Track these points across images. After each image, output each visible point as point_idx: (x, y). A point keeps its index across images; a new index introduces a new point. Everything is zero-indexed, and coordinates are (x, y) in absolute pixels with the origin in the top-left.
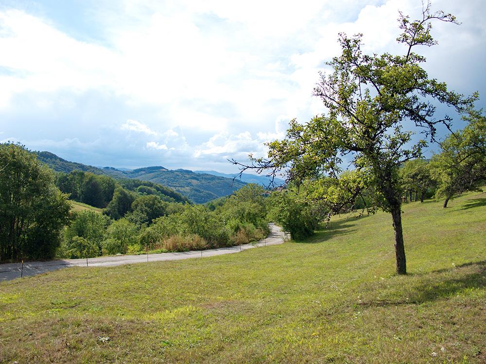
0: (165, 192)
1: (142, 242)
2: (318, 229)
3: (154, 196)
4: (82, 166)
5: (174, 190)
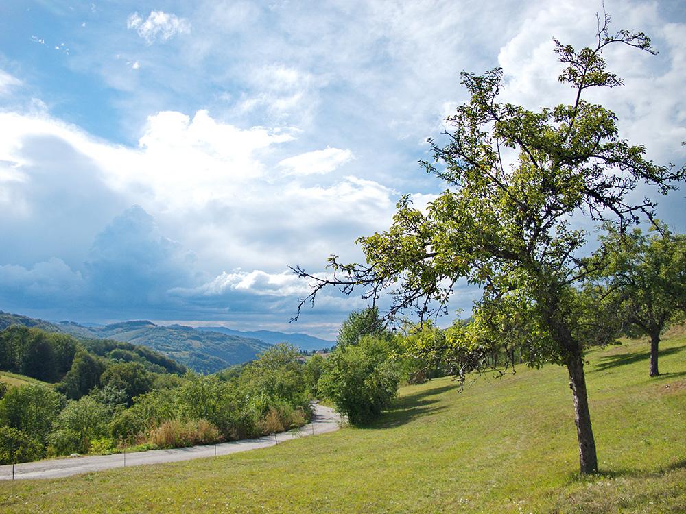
0: (151, 359)
2: (391, 407)
3: (135, 364)
5: (165, 354)
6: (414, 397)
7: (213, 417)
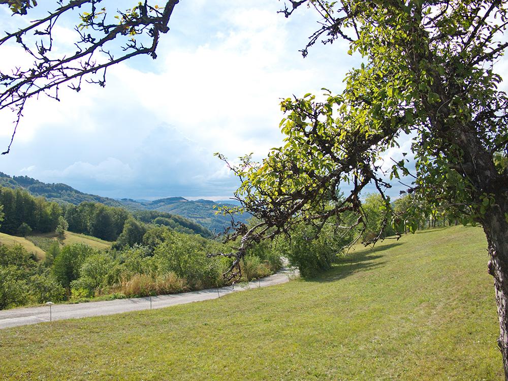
5: (194, 221)
6: (363, 253)
7: (178, 270)
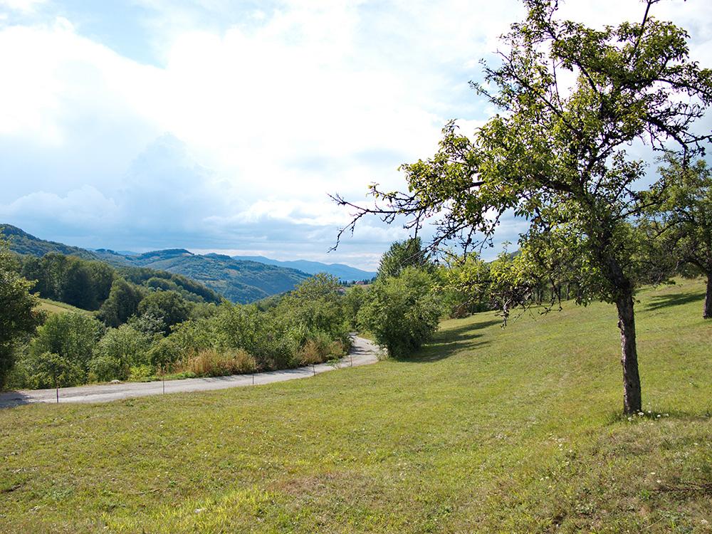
0: (189, 288)
1: (153, 362)
3: (173, 292)
4: (62, 248)
5: (203, 284)
